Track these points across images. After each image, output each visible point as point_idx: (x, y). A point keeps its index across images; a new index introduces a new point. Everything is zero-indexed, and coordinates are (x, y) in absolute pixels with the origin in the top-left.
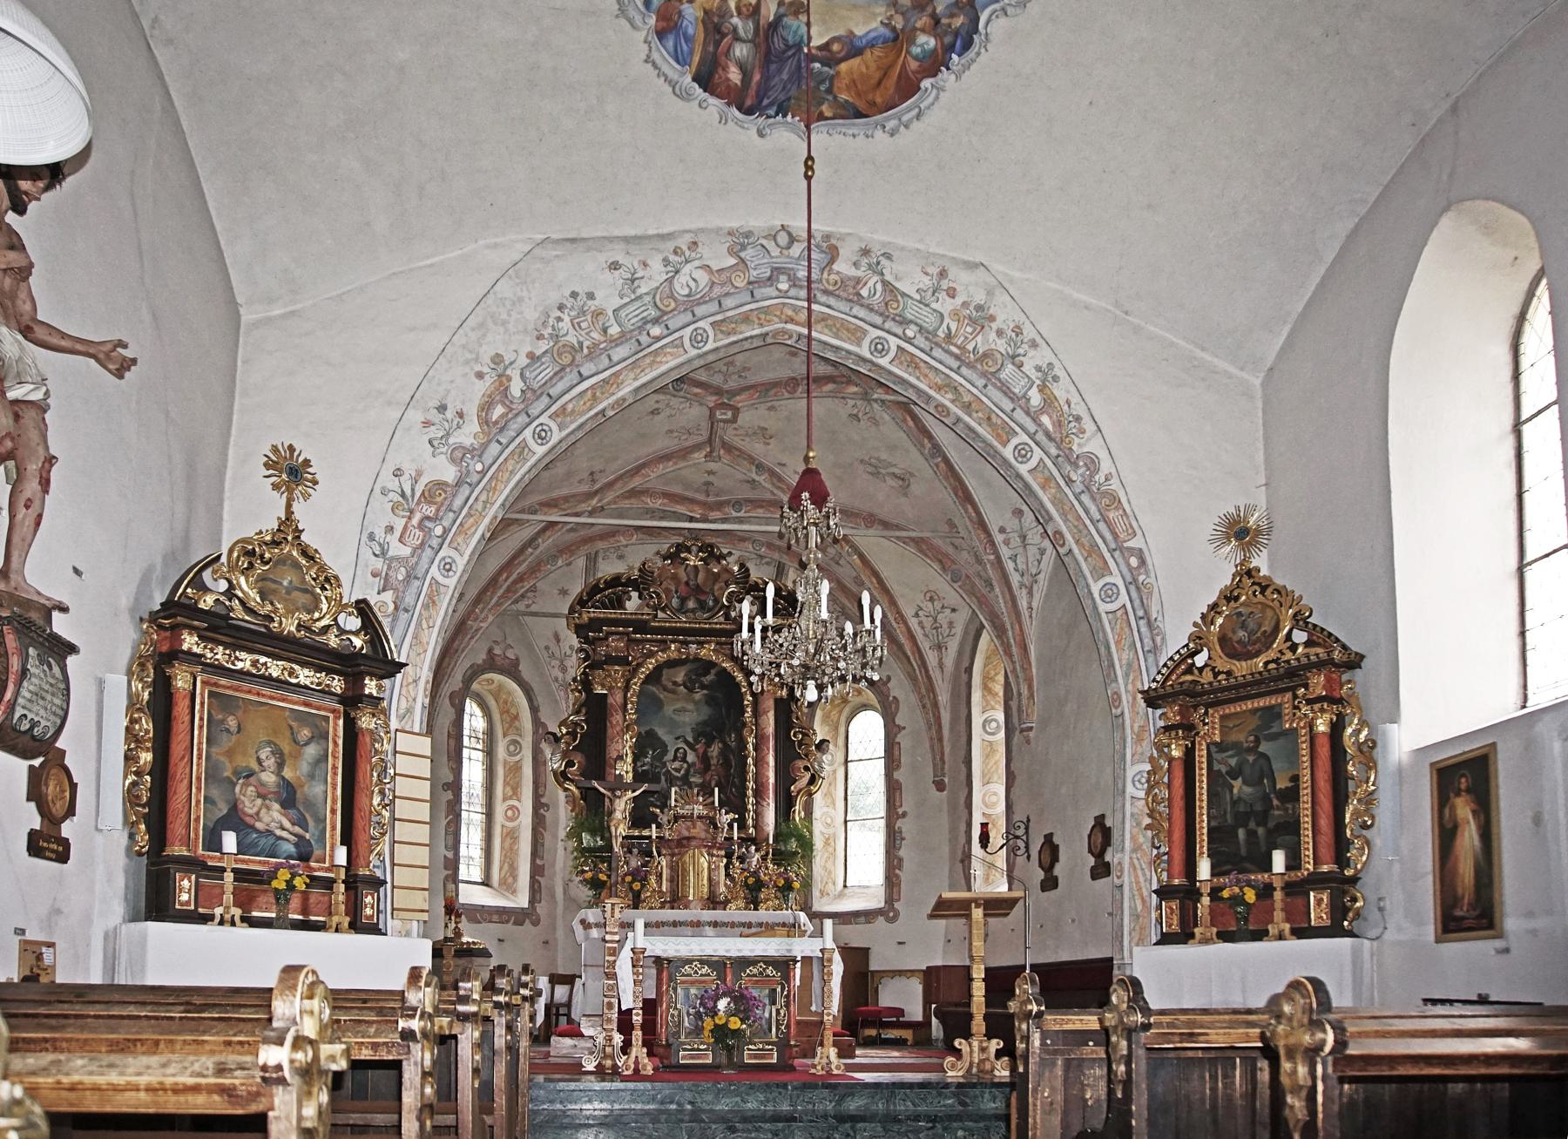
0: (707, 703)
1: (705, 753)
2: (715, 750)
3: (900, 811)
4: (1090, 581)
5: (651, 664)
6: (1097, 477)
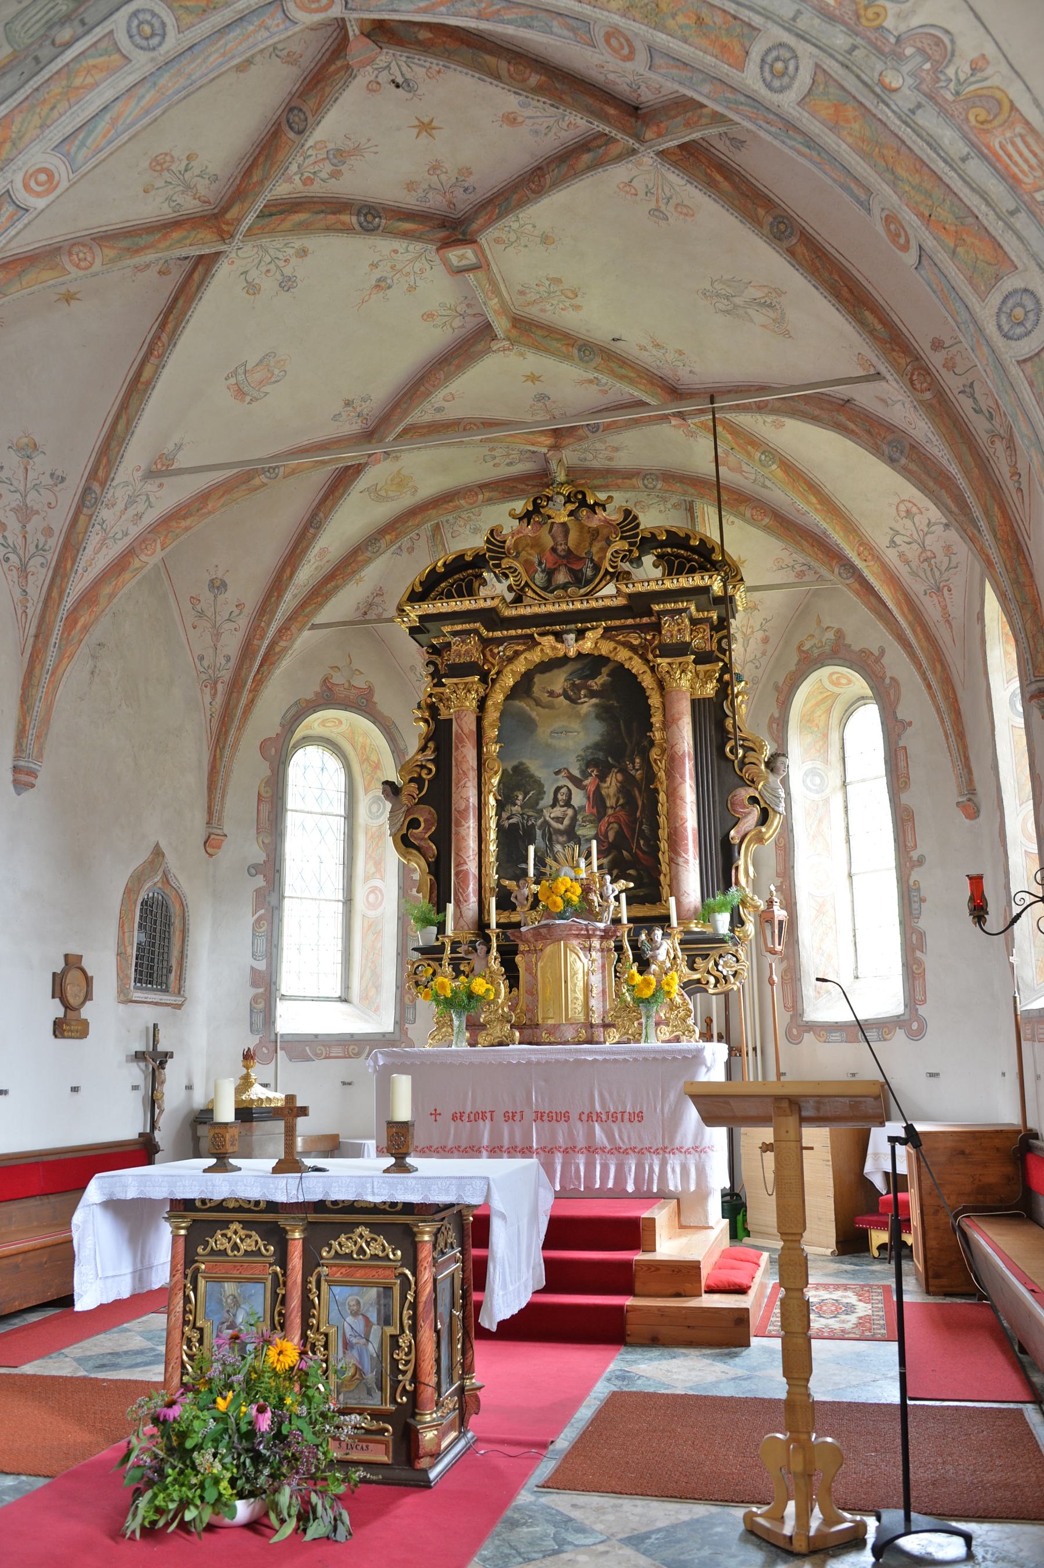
0: (598, 717)
1: (598, 789)
2: (611, 786)
3: (915, 855)
4: (973, 300)
5: (520, 666)
6: (950, 72)
